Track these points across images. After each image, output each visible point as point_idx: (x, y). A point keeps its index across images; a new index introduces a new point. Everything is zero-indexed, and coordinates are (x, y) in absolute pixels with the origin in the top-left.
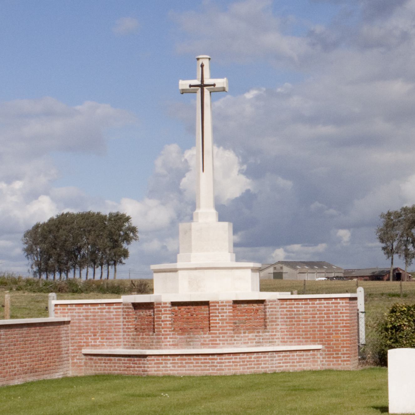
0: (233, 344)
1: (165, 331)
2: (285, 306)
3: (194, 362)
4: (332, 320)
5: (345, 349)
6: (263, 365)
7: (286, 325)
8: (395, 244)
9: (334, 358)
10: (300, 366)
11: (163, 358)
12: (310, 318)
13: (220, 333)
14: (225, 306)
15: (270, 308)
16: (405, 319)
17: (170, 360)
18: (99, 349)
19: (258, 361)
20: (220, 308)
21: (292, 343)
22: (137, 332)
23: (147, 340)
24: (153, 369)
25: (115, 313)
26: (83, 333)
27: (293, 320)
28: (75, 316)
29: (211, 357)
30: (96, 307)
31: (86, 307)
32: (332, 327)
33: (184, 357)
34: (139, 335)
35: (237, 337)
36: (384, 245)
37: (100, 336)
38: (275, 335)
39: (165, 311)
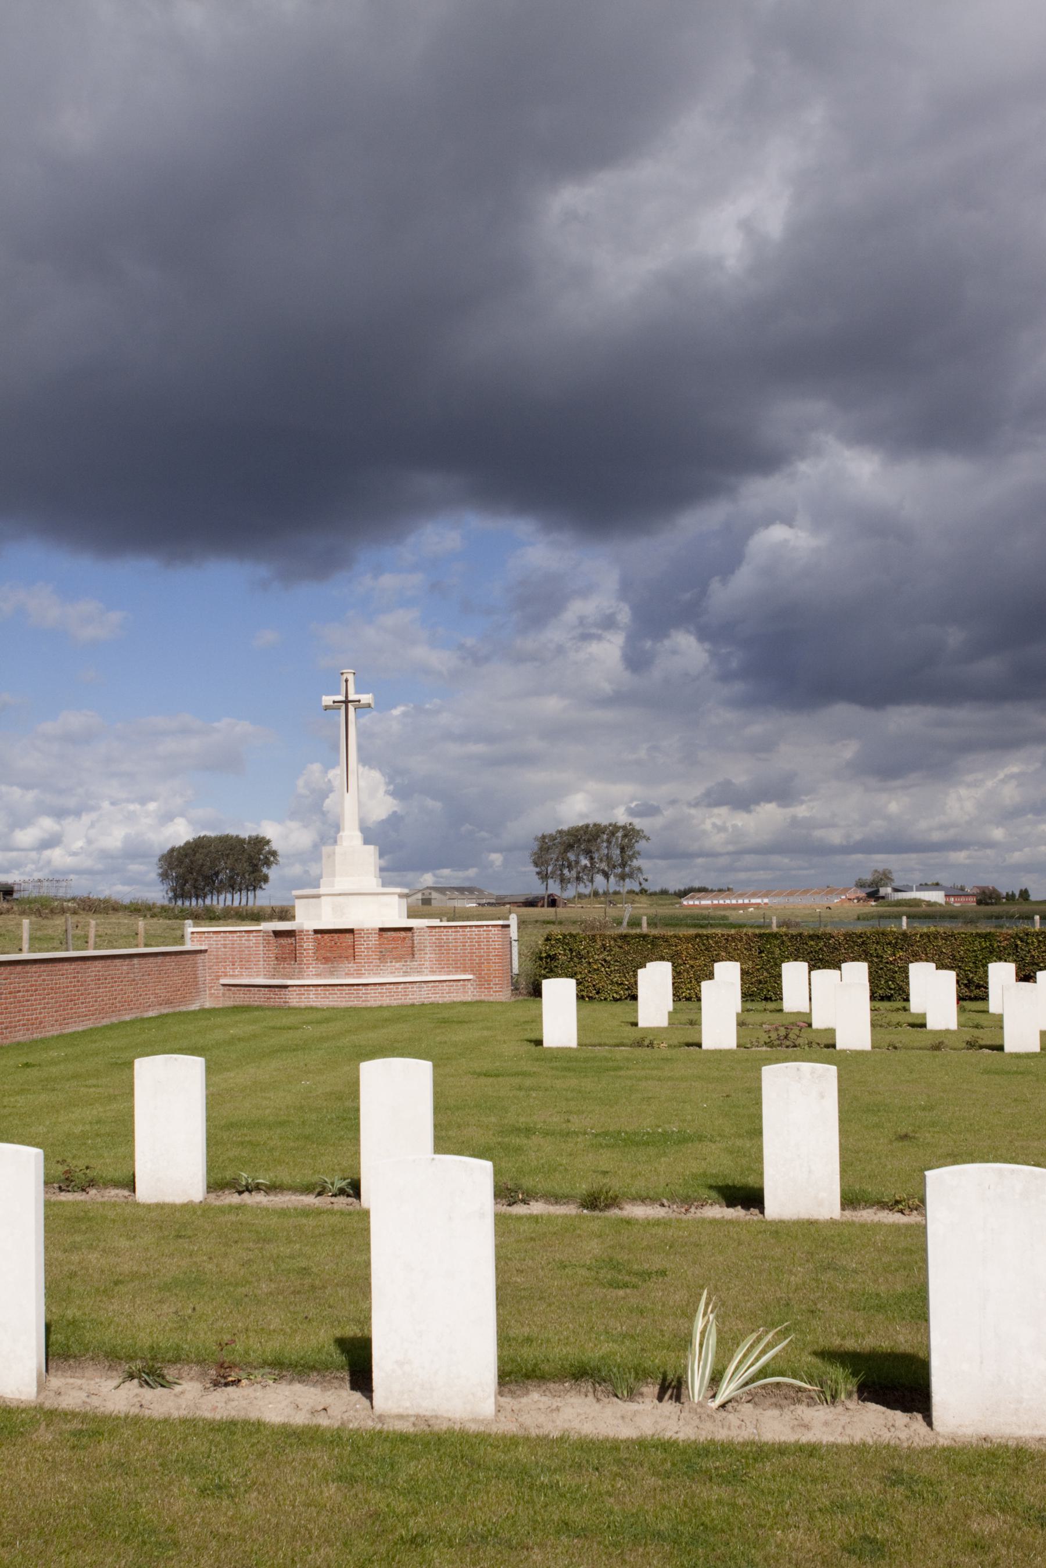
8: (550, 869)
36: (538, 870)
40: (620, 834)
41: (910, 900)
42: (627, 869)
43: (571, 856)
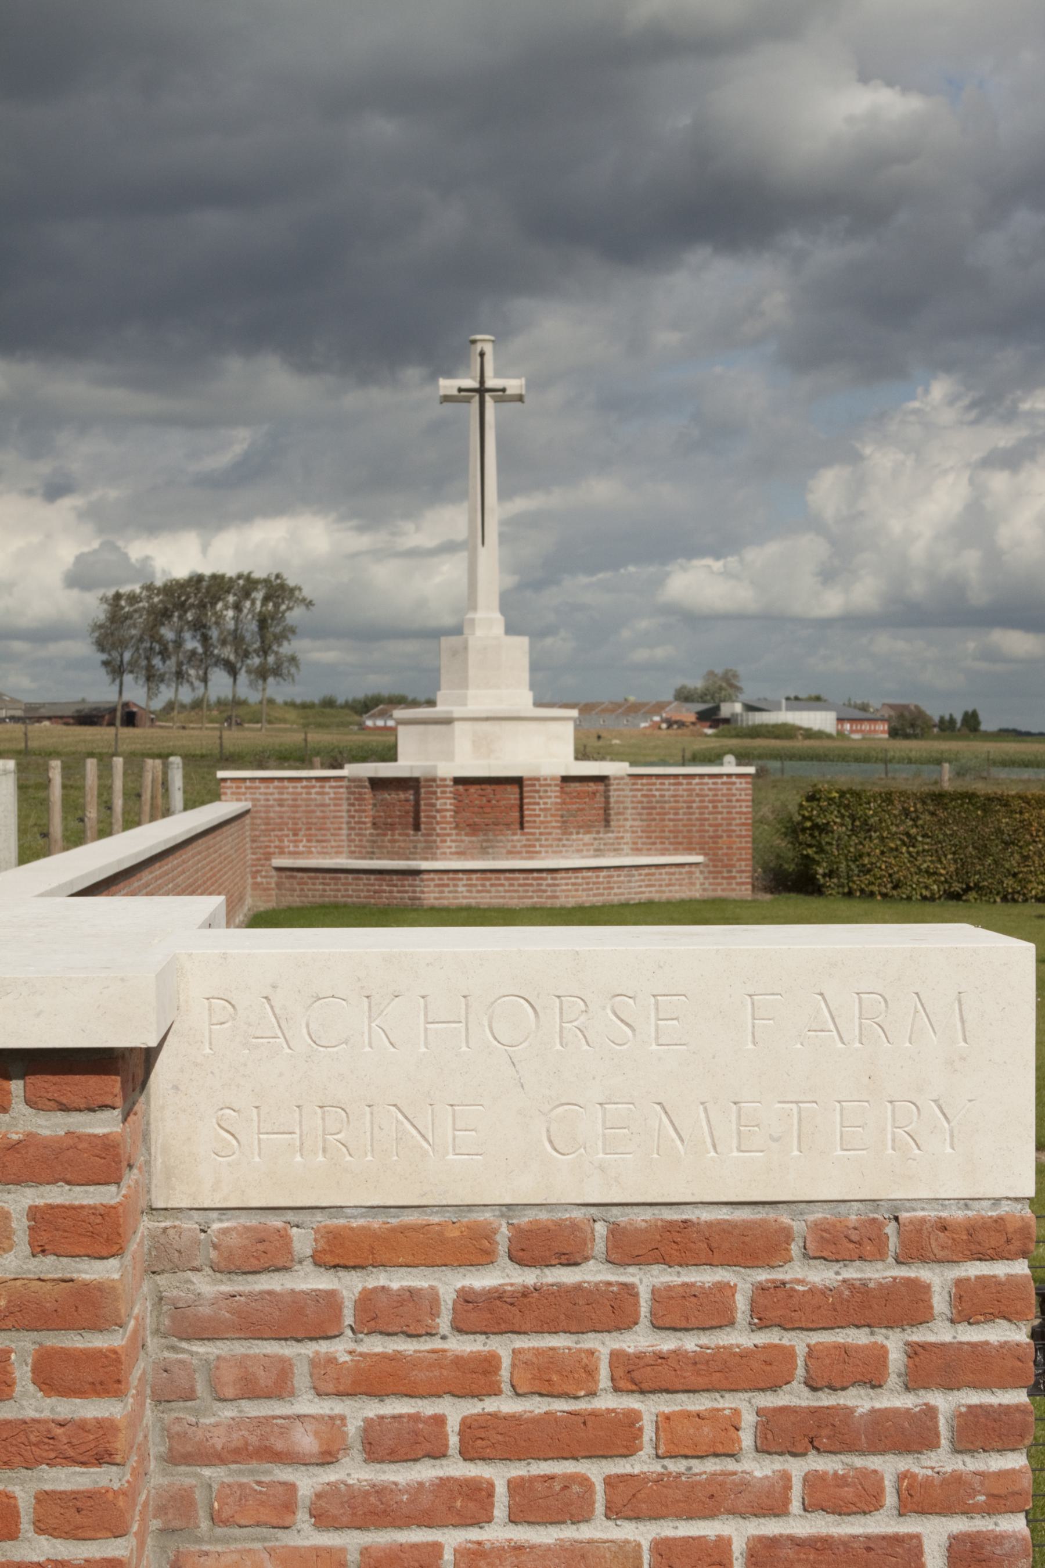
0: (561, 852)
1: (442, 829)
2: (639, 787)
3: (506, 883)
4: (721, 813)
5: (743, 863)
6: (616, 891)
7: (642, 820)
8: (127, 656)
9: (723, 878)
10: (670, 891)
11: (451, 876)
12: (682, 808)
13: (541, 834)
14: (550, 785)
15: (615, 790)
16: (836, 813)
17: (462, 879)
18: (303, 858)
19: (609, 882)
20: (542, 789)
21: (652, 852)
22: (375, 829)
23: (402, 845)
24: (432, 895)
25: (332, 796)
26: (273, 830)
27: (654, 811)
28: (259, 800)
29: (535, 875)
30: (299, 785)
31: (308, 784)
32: (721, 825)
33: (489, 875)
34: (385, 835)
35: (568, 840)
36: (104, 657)
37: (305, 835)
38: (622, 838)
39: (443, 792)
40: (259, 595)
41: (776, 726)
42: (271, 659)
43: (167, 633)
